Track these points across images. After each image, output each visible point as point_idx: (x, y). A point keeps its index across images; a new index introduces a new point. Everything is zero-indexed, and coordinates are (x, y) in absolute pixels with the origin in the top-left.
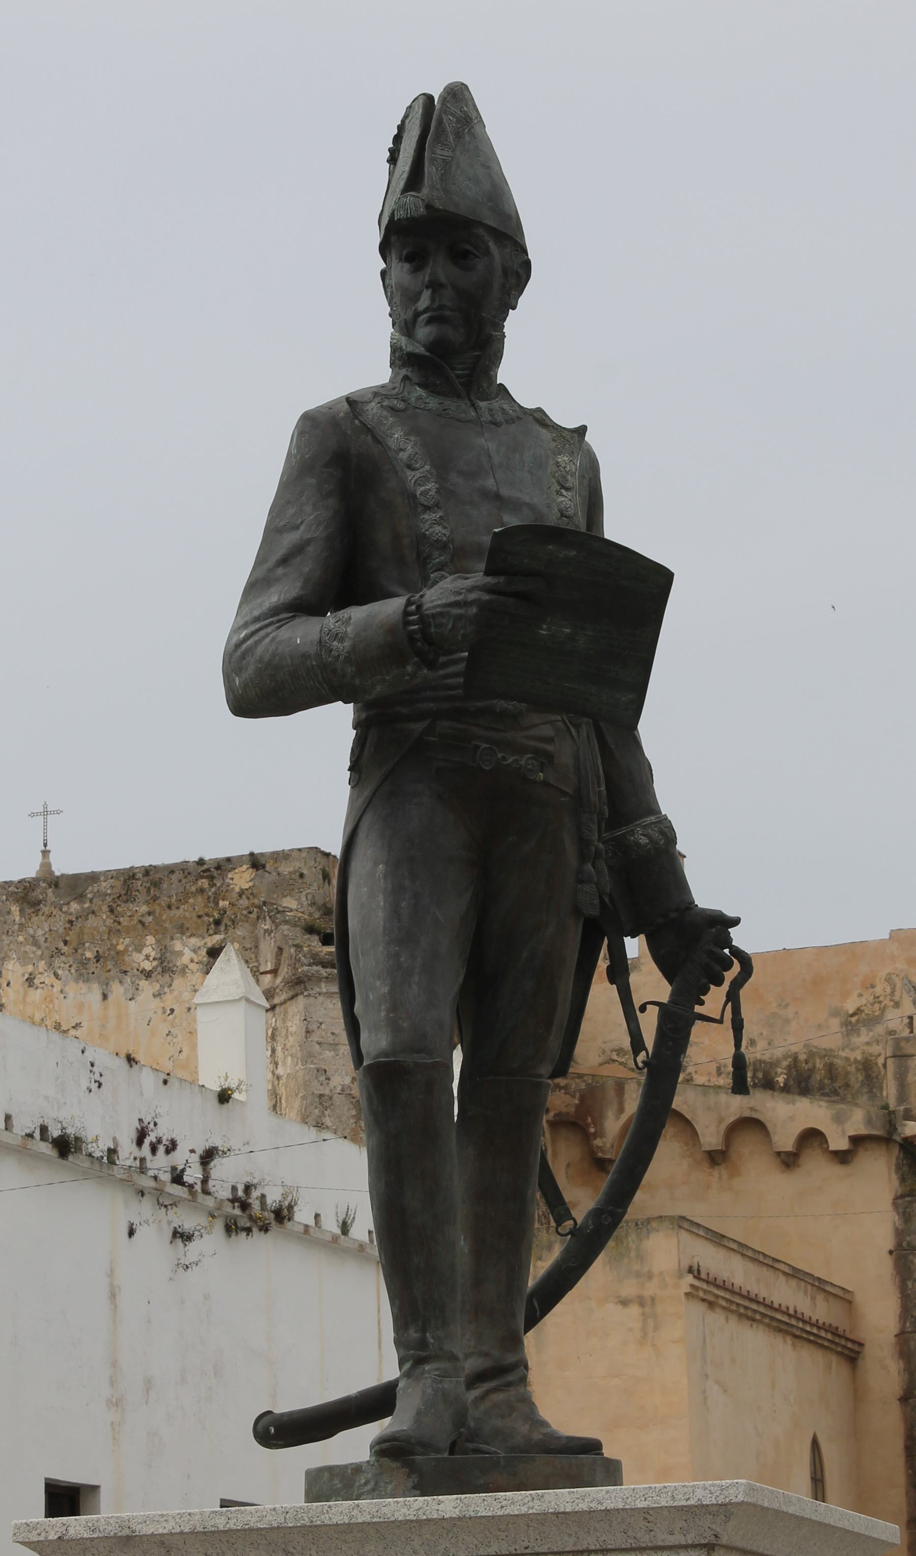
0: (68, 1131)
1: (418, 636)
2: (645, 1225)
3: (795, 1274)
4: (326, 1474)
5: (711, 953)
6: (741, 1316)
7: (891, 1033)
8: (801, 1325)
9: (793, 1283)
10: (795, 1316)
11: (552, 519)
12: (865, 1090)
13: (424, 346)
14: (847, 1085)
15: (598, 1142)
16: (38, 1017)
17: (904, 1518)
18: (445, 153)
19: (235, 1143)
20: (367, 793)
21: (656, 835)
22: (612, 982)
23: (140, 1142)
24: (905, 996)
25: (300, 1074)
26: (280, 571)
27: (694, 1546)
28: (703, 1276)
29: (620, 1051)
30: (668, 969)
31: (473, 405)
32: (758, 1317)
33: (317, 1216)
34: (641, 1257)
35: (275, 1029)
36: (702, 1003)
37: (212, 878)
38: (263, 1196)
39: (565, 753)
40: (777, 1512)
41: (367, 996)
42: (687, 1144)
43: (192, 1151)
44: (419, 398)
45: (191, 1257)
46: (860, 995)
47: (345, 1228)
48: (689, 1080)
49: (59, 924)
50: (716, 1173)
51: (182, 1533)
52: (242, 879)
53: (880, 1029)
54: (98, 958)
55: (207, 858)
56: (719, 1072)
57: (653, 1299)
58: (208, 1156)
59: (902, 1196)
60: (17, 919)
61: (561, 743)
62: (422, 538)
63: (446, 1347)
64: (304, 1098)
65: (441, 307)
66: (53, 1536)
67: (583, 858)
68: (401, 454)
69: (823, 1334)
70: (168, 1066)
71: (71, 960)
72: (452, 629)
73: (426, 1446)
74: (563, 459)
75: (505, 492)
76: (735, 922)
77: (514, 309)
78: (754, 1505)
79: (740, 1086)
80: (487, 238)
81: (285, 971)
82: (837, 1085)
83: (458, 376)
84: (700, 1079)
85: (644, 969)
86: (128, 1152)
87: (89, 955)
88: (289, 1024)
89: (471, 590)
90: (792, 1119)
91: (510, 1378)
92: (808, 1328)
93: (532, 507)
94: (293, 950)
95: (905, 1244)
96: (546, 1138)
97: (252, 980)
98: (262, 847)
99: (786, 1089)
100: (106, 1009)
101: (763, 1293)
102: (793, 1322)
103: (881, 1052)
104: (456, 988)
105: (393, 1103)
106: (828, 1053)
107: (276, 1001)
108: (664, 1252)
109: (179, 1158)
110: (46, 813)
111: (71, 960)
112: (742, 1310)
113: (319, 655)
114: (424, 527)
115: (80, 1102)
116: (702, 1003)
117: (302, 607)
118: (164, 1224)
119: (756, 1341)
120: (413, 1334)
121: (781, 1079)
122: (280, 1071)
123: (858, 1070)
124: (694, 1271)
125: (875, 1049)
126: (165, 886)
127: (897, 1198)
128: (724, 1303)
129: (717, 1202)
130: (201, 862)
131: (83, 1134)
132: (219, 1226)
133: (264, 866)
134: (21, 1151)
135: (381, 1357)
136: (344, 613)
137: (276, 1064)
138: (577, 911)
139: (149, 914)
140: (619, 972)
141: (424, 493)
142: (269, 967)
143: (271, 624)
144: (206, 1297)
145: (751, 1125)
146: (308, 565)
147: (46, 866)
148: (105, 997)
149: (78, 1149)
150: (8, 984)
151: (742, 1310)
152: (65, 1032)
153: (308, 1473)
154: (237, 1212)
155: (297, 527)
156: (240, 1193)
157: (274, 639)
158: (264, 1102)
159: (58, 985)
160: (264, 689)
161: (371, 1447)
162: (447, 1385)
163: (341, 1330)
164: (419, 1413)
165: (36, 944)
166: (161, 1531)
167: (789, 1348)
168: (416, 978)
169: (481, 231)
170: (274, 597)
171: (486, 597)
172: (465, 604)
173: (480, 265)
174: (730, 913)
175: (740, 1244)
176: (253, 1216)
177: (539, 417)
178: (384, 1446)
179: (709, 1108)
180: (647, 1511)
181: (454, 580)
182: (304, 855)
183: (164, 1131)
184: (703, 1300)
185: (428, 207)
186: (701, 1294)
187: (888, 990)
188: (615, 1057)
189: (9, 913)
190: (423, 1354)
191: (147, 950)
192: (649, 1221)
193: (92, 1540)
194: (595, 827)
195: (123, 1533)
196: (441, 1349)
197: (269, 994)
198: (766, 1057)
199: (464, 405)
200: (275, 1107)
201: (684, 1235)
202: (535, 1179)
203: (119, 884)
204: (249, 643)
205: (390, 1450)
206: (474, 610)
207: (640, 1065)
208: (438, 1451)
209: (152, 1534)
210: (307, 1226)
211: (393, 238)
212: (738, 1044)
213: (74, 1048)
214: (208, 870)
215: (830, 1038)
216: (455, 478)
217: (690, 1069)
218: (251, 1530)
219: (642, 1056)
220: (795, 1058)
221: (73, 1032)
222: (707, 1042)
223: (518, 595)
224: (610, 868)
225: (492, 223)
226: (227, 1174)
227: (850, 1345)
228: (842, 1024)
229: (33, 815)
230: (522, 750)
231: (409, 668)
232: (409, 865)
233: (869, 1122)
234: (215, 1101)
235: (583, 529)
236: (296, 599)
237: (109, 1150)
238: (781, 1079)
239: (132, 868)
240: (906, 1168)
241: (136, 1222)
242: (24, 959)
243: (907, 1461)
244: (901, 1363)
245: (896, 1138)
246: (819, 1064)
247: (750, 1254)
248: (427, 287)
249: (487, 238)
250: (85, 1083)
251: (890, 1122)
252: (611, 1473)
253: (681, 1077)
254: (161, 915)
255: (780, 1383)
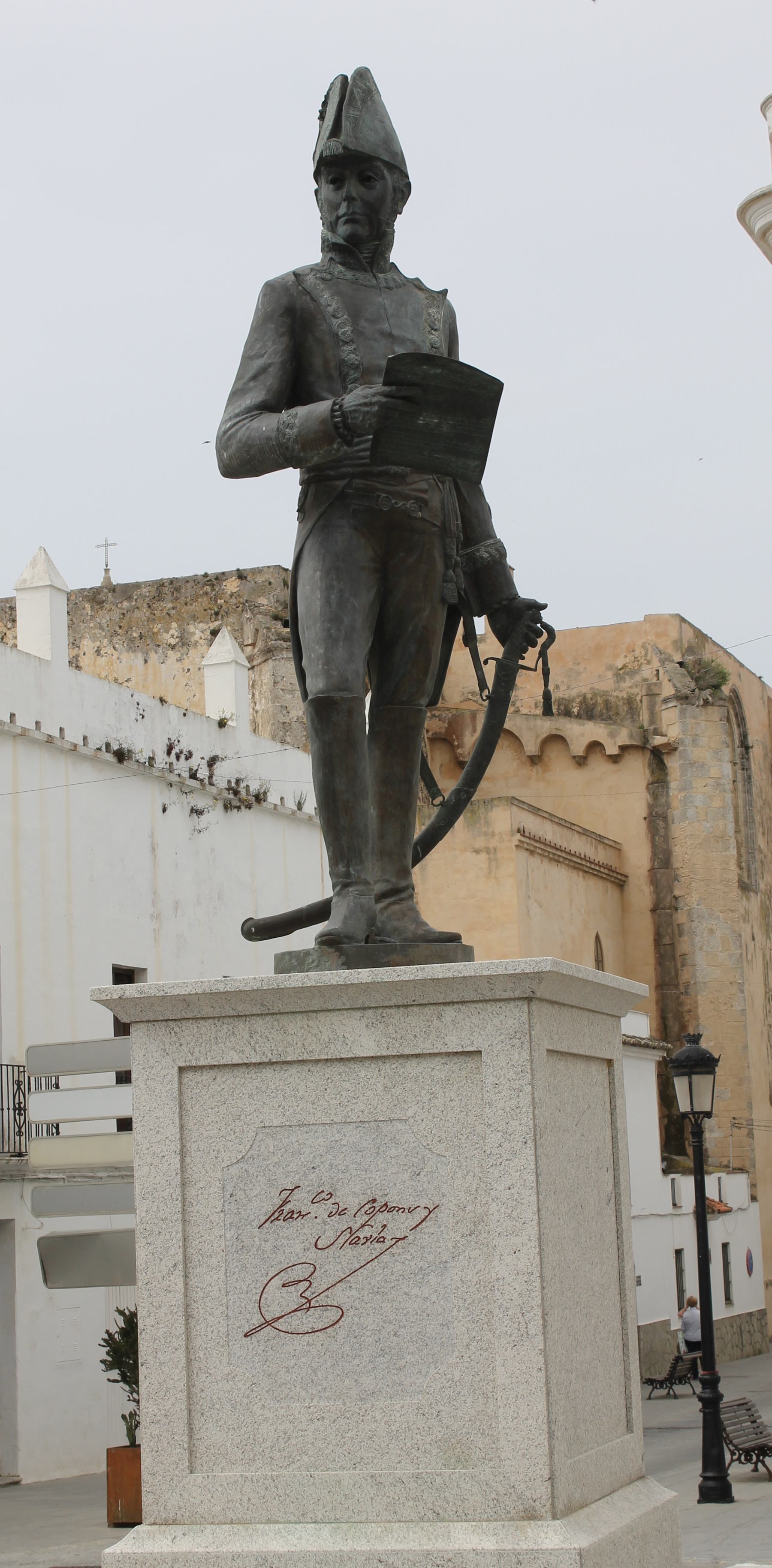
0: (123, 746)
1: (341, 425)
2: (489, 803)
3: (585, 832)
4: (287, 957)
5: (529, 627)
6: (550, 859)
7: (645, 680)
8: (588, 864)
9: (584, 838)
10: (584, 859)
11: (426, 349)
12: (629, 716)
13: (343, 238)
14: (618, 714)
15: (460, 751)
16: (103, 675)
17: (654, 984)
18: (355, 113)
19: (229, 753)
20: (309, 525)
21: (493, 552)
22: (466, 645)
23: (169, 753)
24: (654, 656)
25: (271, 709)
26: (252, 384)
27: (519, 999)
28: (527, 834)
29: (473, 693)
30: (502, 635)
31: (375, 276)
32: (561, 860)
33: (282, 799)
34: (487, 823)
35: (254, 681)
36: (523, 658)
37: (213, 585)
38: (248, 786)
39: (435, 500)
40: (572, 977)
41: (310, 655)
42: (516, 752)
43: (202, 758)
44: (341, 272)
45: (202, 825)
46: (626, 656)
47: (300, 806)
48: (517, 711)
49: (116, 615)
50: (534, 770)
51: (197, 994)
52: (232, 586)
53: (638, 678)
54: (141, 637)
55: (209, 573)
56: (536, 706)
57: (495, 849)
58: (212, 762)
59: (652, 783)
60: (89, 612)
61: (434, 494)
62: (342, 362)
63: (362, 876)
64: (273, 724)
65: (354, 213)
66: (115, 996)
67: (447, 567)
68: (329, 308)
69: (602, 870)
70: (187, 705)
71: (124, 638)
72: (362, 421)
73: (350, 938)
74: (432, 311)
75: (395, 332)
76: (544, 607)
77: (400, 213)
78: (557, 973)
79: (547, 711)
80: (382, 168)
81: (260, 644)
82: (611, 713)
83: (365, 258)
84: (524, 711)
85: (488, 641)
86: (161, 759)
87: (135, 635)
88: (263, 678)
89: (374, 395)
90: (582, 735)
91: (403, 895)
92: (593, 866)
93: (413, 342)
94: (265, 631)
95: (654, 813)
96: (425, 747)
97: (239, 650)
98: (244, 565)
99: (579, 716)
100: (146, 669)
101: (564, 845)
102: (584, 863)
103: (639, 692)
104: (367, 650)
105: (327, 717)
106: (605, 693)
107: (255, 663)
108: (502, 819)
109: (194, 762)
110: (106, 545)
111: (124, 638)
112: (551, 856)
113: (277, 438)
114: (344, 355)
115: (130, 728)
116: (523, 658)
117: (266, 407)
118: (185, 804)
119: (560, 875)
120: (342, 868)
121: (575, 710)
122: (258, 707)
123: (624, 704)
124: (521, 831)
125: (635, 691)
126: (183, 591)
127: (648, 784)
128: (540, 851)
129: (534, 788)
130: (206, 575)
131: (132, 748)
132: (220, 805)
133: (246, 578)
134: (94, 759)
135: (323, 887)
136: (293, 411)
137: (255, 703)
138: (443, 600)
139: (173, 608)
140: (470, 639)
141: (344, 333)
142: (250, 642)
143: (247, 418)
144: (212, 850)
145: (556, 739)
146: (271, 380)
147: (107, 579)
148: (146, 661)
149: (130, 758)
150: (84, 654)
151: (551, 856)
152: (121, 684)
153: (276, 956)
154: (231, 796)
155: (263, 356)
156: (233, 785)
157: (248, 428)
158: (247, 727)
159: (116, 654)
160: (243, 461)
161: (316, 939)
162: (363, 900)
163: (297, 868)
164: (345, 918)
165: (101, 628)
166: (183, 993)
167: (581, 879)
168: (341, 644)
169: (379, 164)
170: (249, 400)
171: (384, 400)
172: (371, 404)
173: (379, 186)
174: (541, 601)
175: (550, 814)
176: (241, 799)
177: (417, 284)
178: (324, 939)
179: (530, 729)
180: (489, 977)
181: (363, 389)
182: (271, 570)
183: (184, 746)
184: (527, 849)
185: (345, 148)
186: (525, 846)
187: (643, 653)
188: (470, 697)
189: (84, 608)
190: (348, 881)
191: (172, 632)
192: (492, 800)
193: (140, 998)
194: (454, 547)
195: (160, 994)
196: (359, 878)
197: (250, 659)
198: (566, 696)
199: (369, 276)
200: (255, 730)
201: (514, 809)
202: (418, 770)
203: (153, 590)
204: (232, 430)
205: (328, 941)
206: (376, 408)
207: (485, 698)
208: (358, 942)
209: (178, 995)
210: (275, 805)
211: (322, 169)
212: (546, 684)
213: (126, 694)
214: (210, 580)
215: (607, 684)
216: (363, 323)
217: (518, 704)
218: (240, 991)
219: (486, 692)
220: (585, 697)
221: (125, 684)
222: (528, 687)
223: (405, 398)
224: (464, 573)
225: (386, 158)
226: (224, 773)
227: (619, 877)
228: (614, 675)
229: (98, 546)
230: (407, 498)
231: (335, 446)
232: (336, 570)
233: (631, 736)
234: (216, 726)
235: (446, 355)
236: (262, 402)
237: (150, 758)
238: (575, 710)
239: (162, 579)
240: (654, 766)
241: (168, 803)
242: (94, 638)
243: (655, 949)
244: (652, 888)
245: (649, 746)
246: (600, 700)
247: (556, 820)
248: (345, 200)
249: (382, 168)
250: (133, 716)
251: (644, 736)
252: (467, 954)
253: (511, 709)
254: (180, 609)
255: (576, 902)
